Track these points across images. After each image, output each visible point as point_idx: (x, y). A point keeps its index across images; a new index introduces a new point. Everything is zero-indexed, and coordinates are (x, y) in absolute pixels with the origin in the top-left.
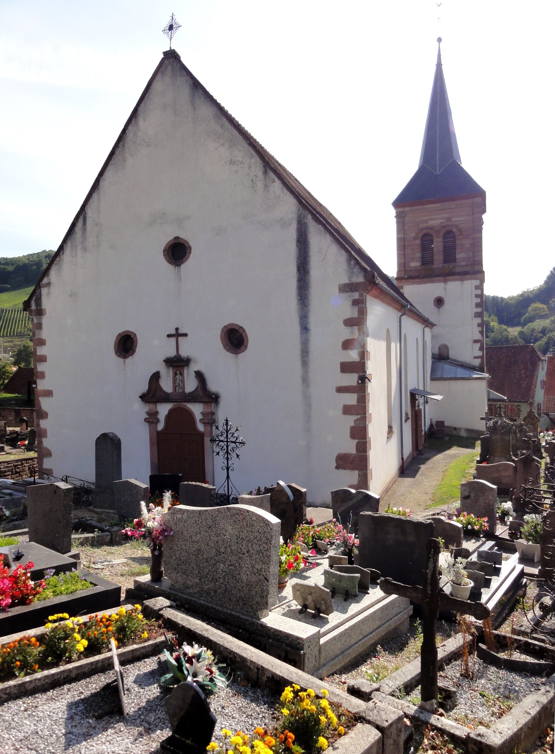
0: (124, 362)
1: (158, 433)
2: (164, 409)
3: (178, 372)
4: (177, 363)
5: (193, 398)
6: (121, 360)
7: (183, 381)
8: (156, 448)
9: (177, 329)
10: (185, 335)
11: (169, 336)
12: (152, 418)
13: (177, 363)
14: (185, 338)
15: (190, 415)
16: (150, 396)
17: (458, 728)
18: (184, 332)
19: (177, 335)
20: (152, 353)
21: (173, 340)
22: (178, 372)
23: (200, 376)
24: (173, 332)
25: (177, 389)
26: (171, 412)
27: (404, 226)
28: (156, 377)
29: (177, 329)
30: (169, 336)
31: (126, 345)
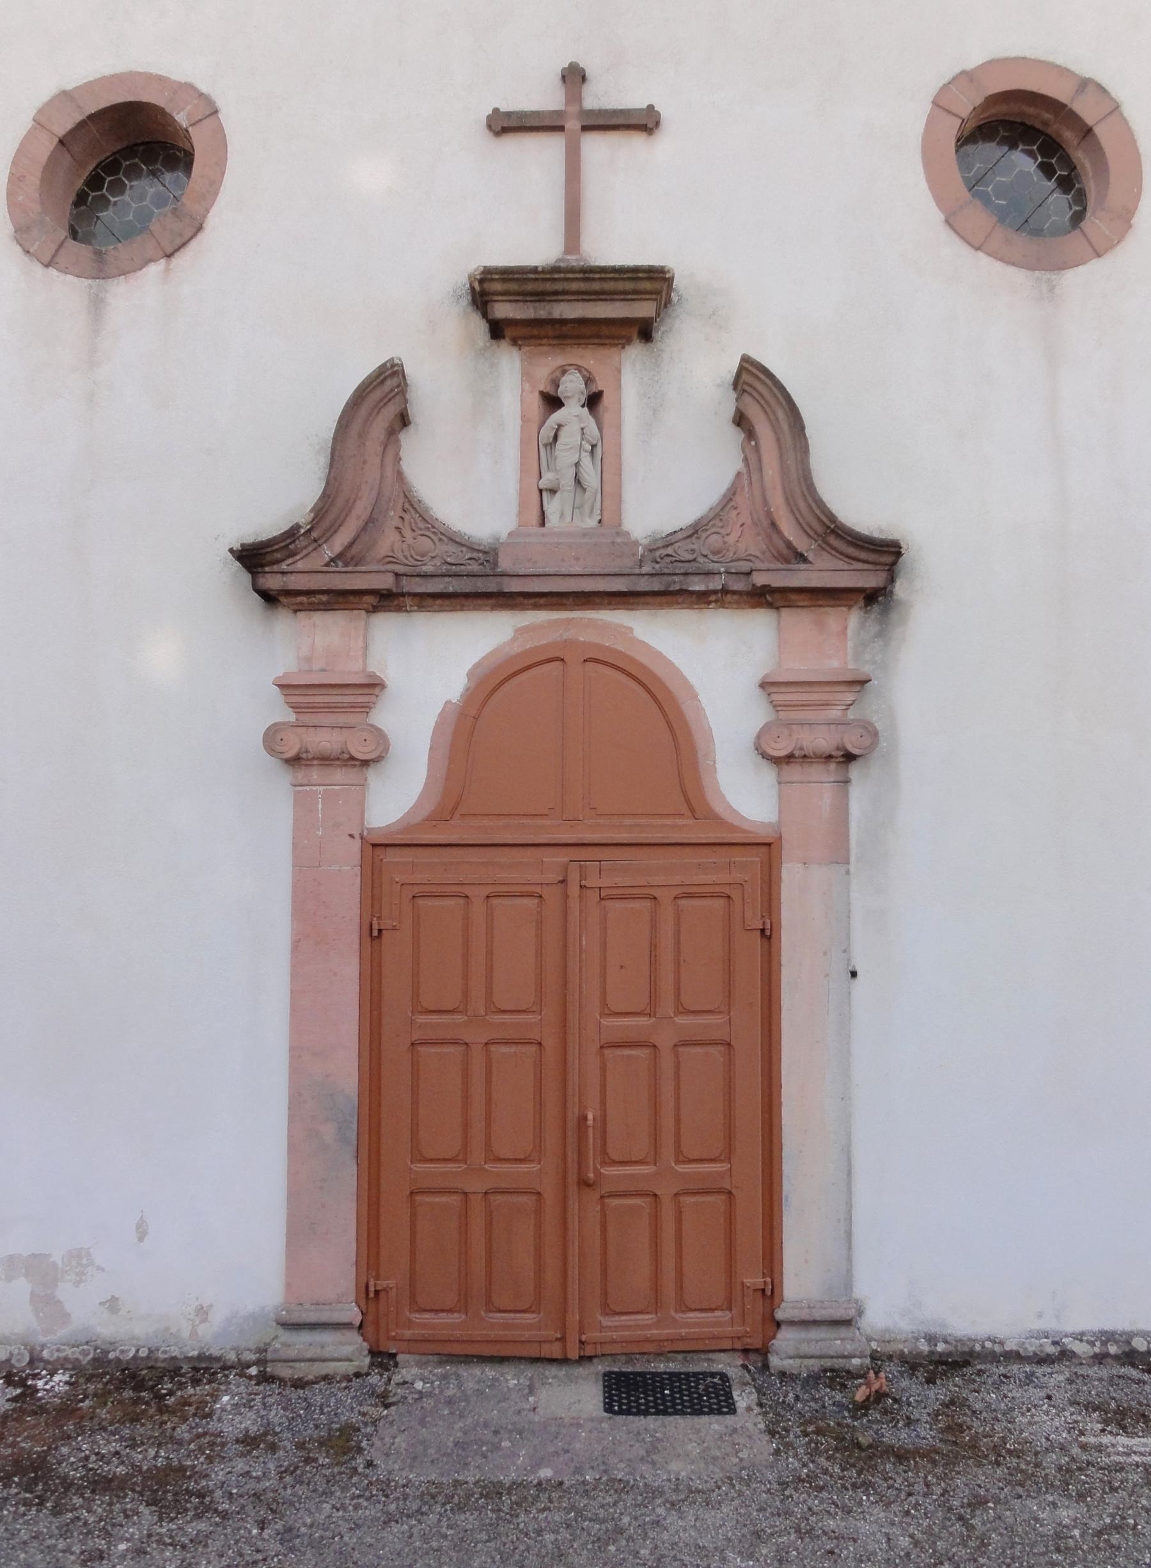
0: (97, 305)
1: (377, 848)
2: (429, 666)
3: (572, 386)
4: (568, 316)
5: (673, 579)
6: (66, 290)
7: (603, 451)
8: (347, 970)
9: (574, 77)
10: (644, 123)
11: (507, 125)
12: (322, 732)
13: (568, 316)
14: (636, 142)
15: (659, 702)
16: (328, 552)
17: (809, 1341)
18: (634, 100)
19: (579, 118)
20: (349, 233)
21: (542, 155)
22: (572, 386)
23: (759, 397)
24: (545, 97)
25: (553, 507)
26: (493, 684)
27: (468, 547)
28: (382, 403)
29: (574, 77)
30: (507, 125)
31: (125, 162)
